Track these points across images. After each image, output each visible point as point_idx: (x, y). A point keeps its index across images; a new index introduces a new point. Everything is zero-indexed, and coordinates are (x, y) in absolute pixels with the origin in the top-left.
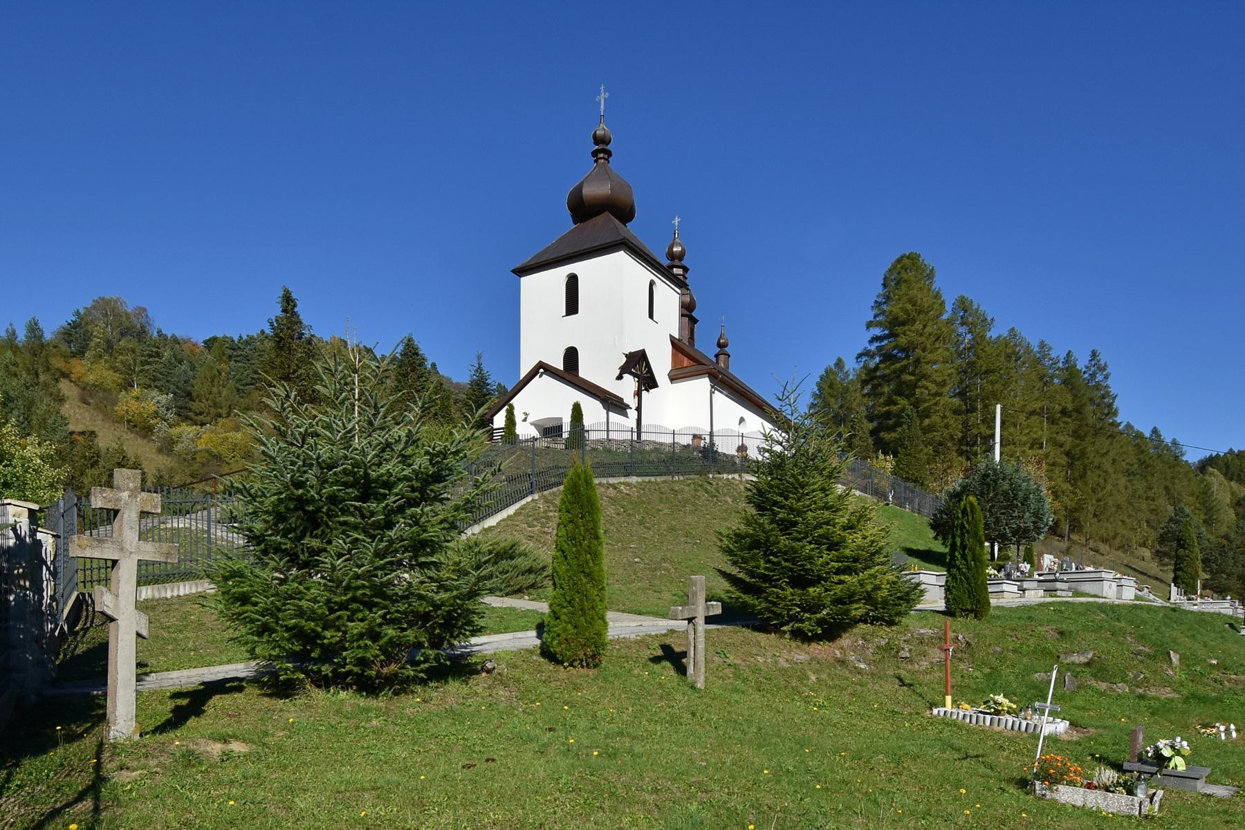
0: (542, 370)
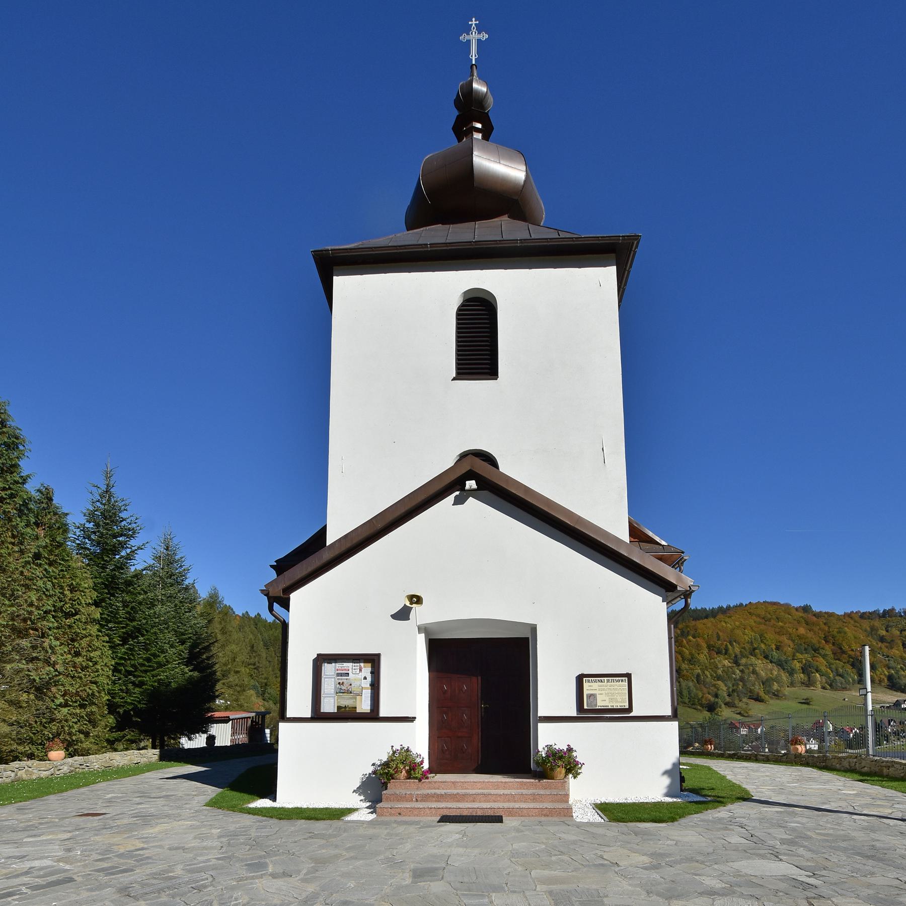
0: (471, 484)
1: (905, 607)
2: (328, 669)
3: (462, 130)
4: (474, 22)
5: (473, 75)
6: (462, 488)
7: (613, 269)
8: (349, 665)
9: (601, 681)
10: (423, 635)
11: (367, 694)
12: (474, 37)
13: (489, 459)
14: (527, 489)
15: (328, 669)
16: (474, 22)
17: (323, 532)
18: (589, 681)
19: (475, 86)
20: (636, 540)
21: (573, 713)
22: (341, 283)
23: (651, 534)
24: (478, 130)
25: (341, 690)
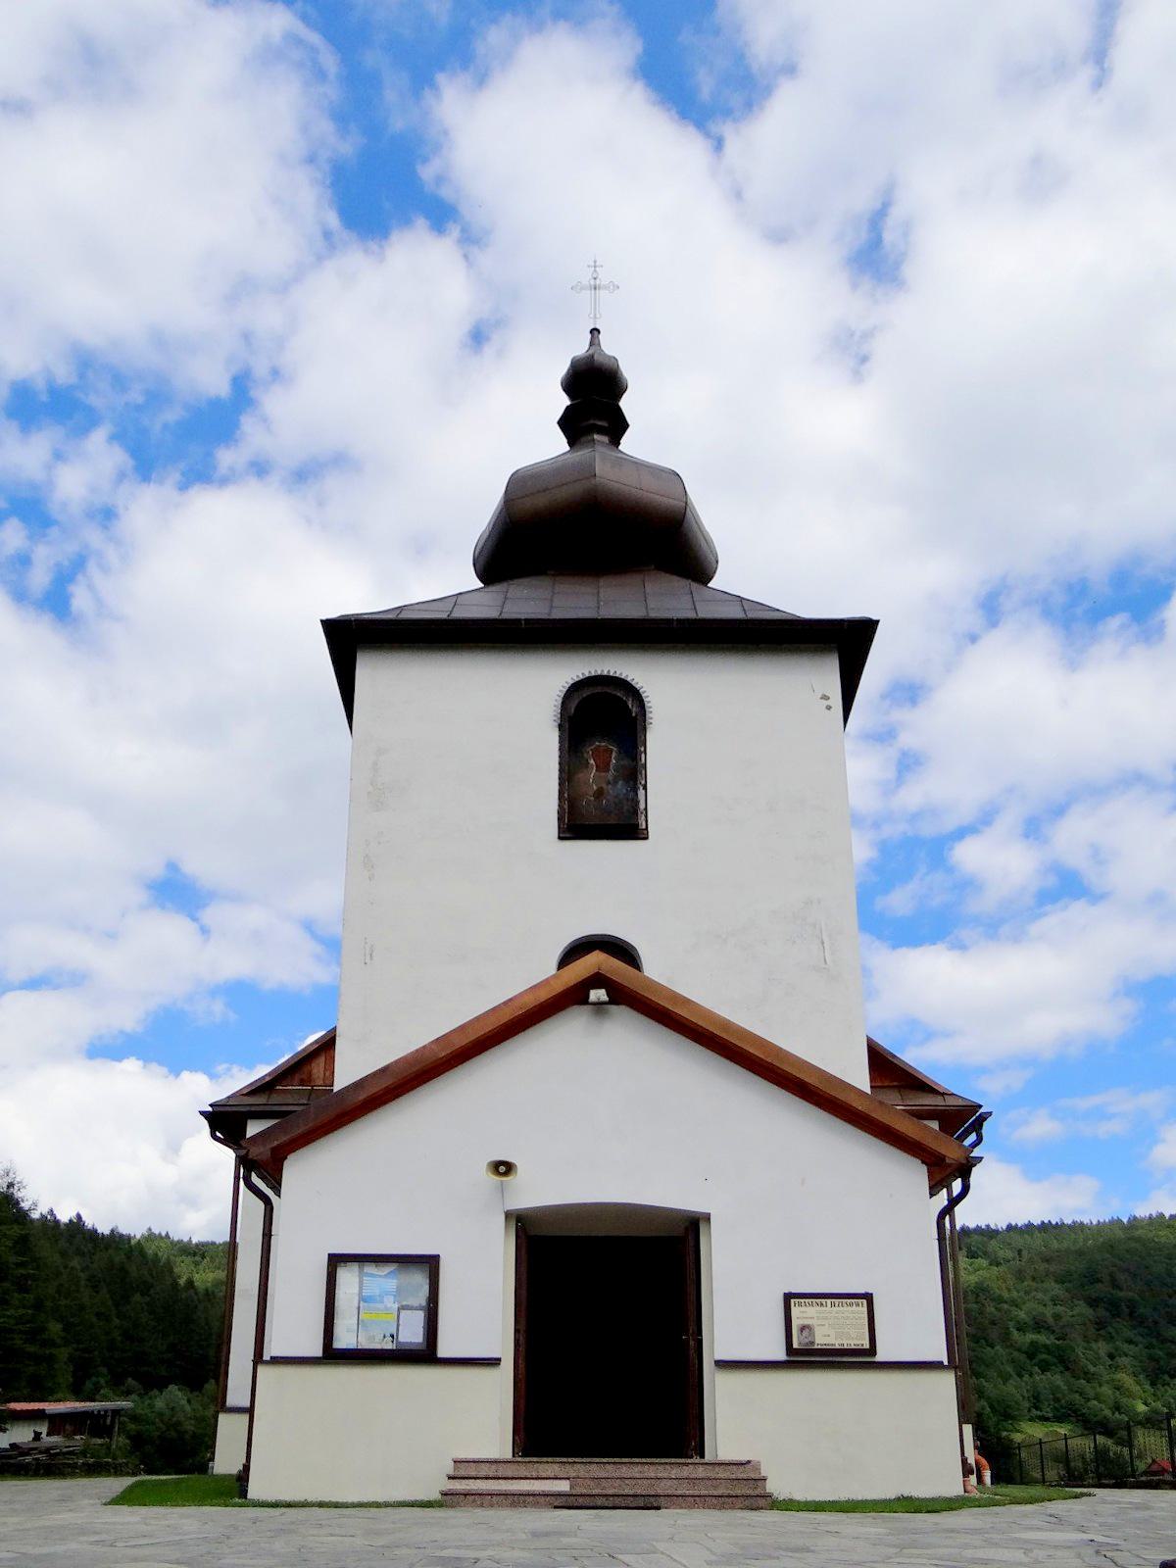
0: (598, 994)
1: (1174, 1213)
2: (347, 1277)
9: (822, 1304)
13: (622, 951)
18: (800, 1305)
20: (895, 1083)
21: (780, 1354)
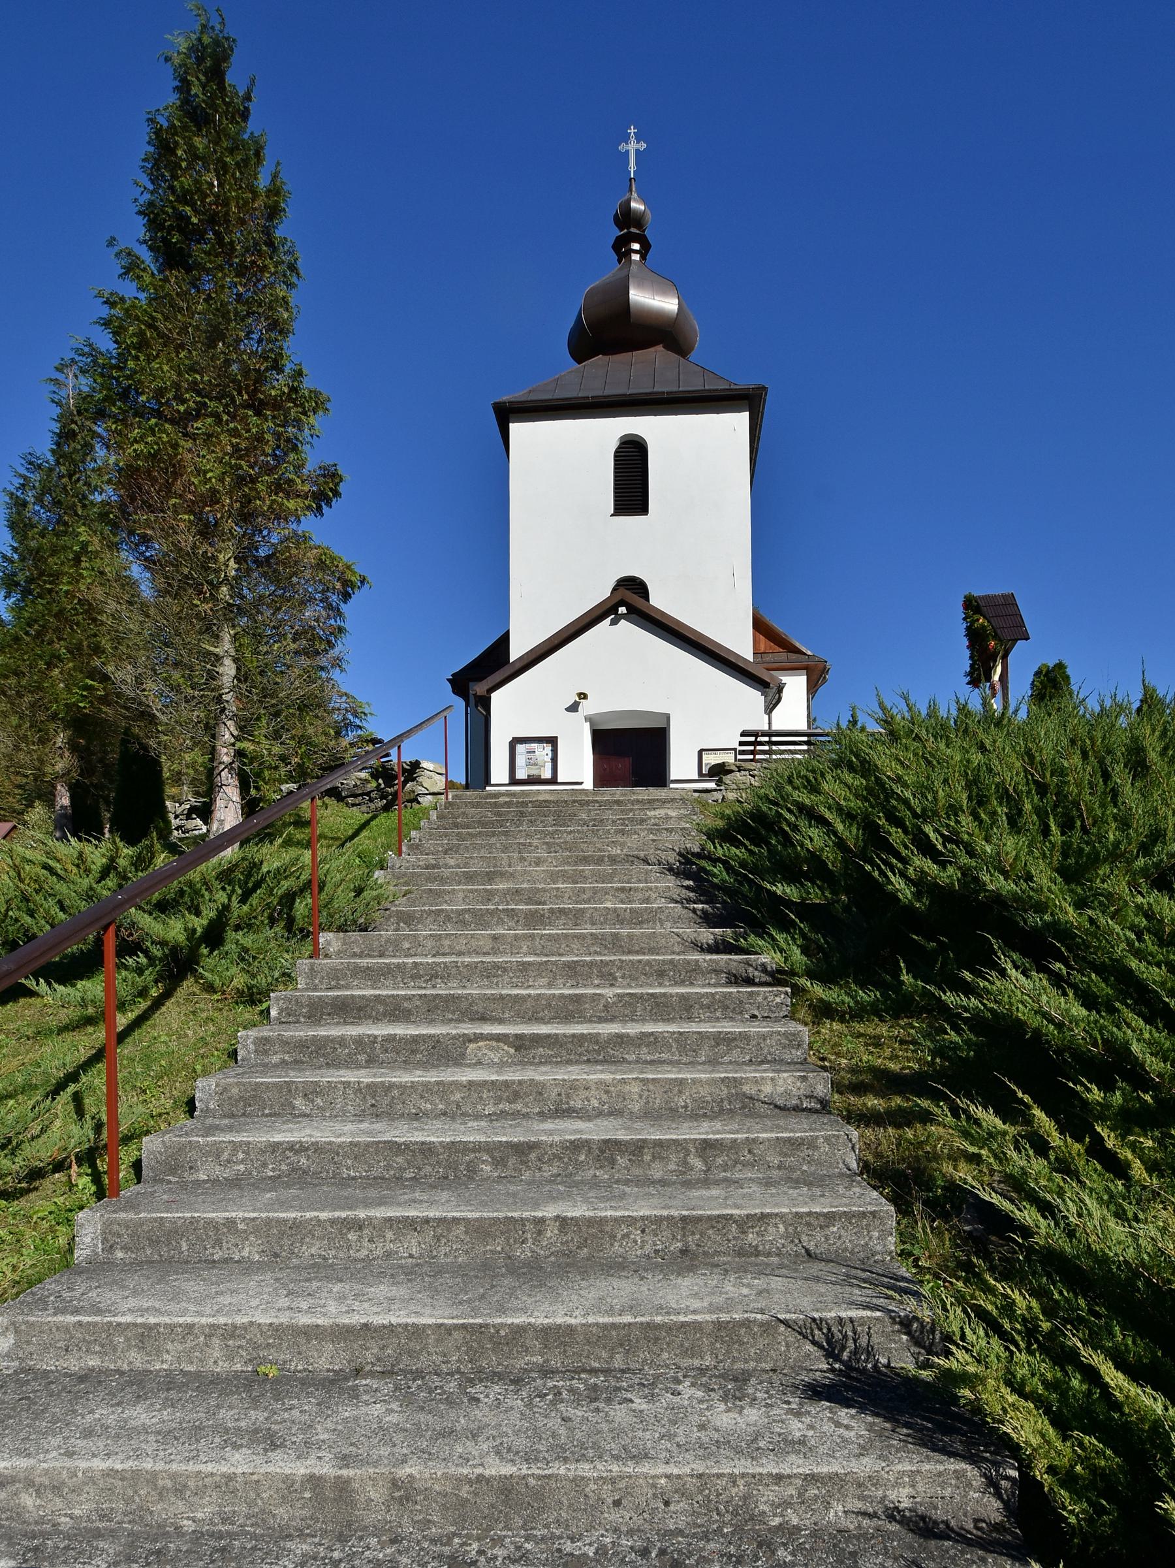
0: (622, 610)
2: (521, 749)
3: (621, 248)
4: (632, 130)
5: (630, 190)
6: (616, 613)
7: (745, 416)
8: (535, 745)
10: (588, 724)
11: (549, 766)
12: (633, 147)
14: (663, 613)
15: (521, 749)
16: (632, 130)
17: (504, 641)
19: (633, 205)
21: (696, 777)
22: (514, 428)
23: (798, 645)
24: (636, 252)
25: (531, 764)
